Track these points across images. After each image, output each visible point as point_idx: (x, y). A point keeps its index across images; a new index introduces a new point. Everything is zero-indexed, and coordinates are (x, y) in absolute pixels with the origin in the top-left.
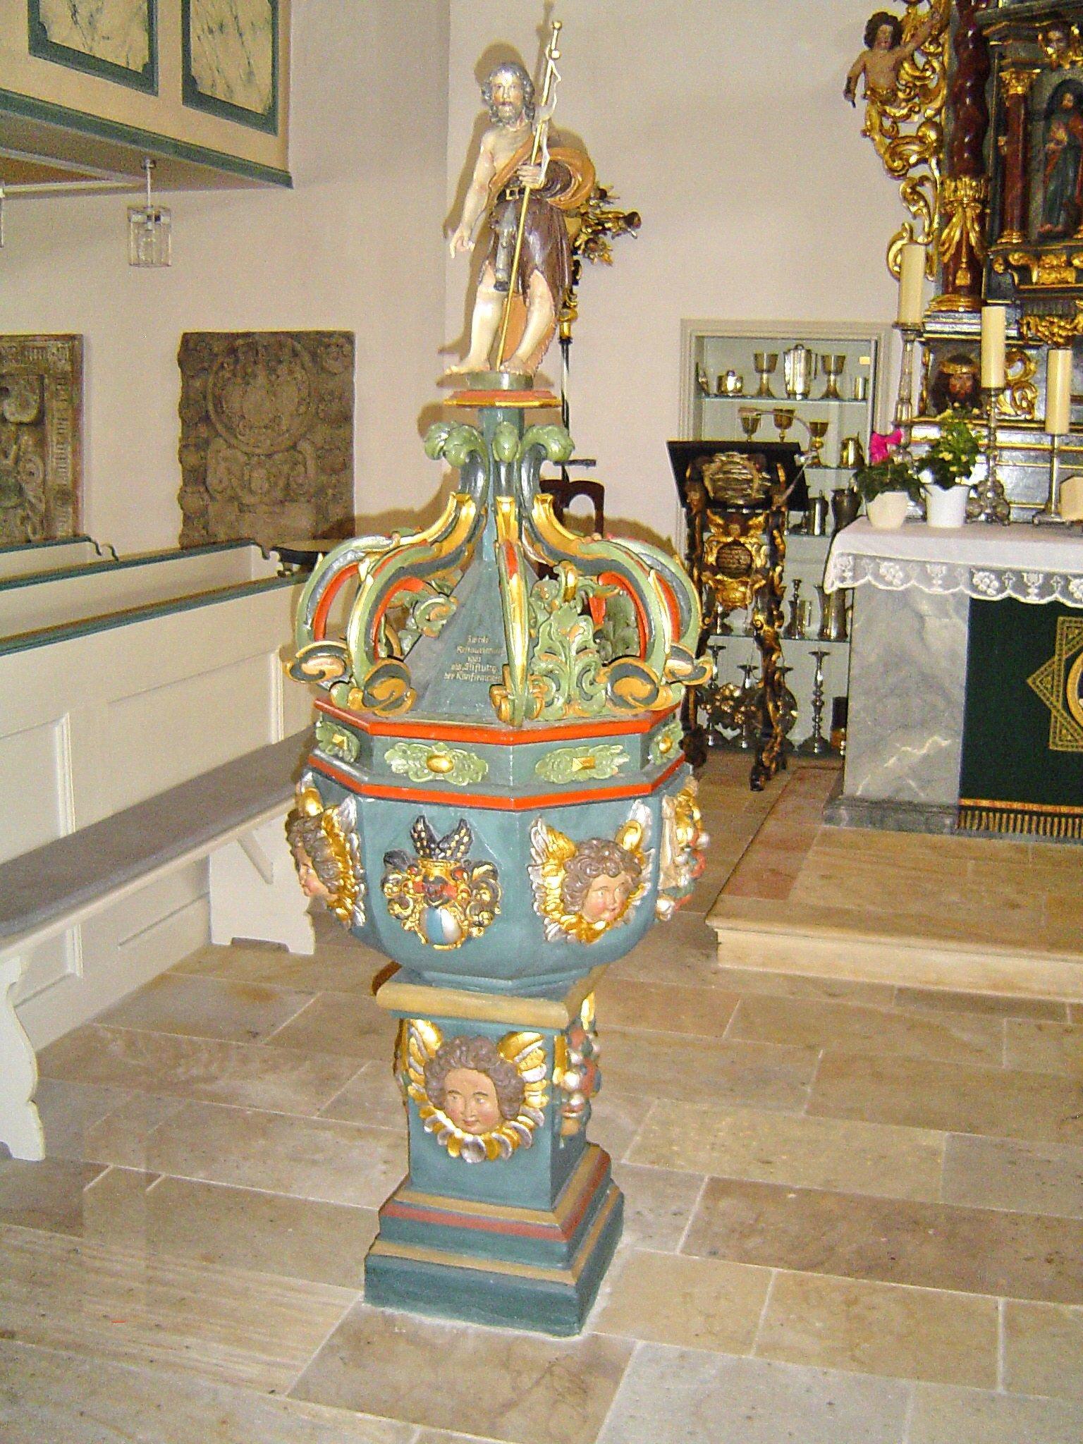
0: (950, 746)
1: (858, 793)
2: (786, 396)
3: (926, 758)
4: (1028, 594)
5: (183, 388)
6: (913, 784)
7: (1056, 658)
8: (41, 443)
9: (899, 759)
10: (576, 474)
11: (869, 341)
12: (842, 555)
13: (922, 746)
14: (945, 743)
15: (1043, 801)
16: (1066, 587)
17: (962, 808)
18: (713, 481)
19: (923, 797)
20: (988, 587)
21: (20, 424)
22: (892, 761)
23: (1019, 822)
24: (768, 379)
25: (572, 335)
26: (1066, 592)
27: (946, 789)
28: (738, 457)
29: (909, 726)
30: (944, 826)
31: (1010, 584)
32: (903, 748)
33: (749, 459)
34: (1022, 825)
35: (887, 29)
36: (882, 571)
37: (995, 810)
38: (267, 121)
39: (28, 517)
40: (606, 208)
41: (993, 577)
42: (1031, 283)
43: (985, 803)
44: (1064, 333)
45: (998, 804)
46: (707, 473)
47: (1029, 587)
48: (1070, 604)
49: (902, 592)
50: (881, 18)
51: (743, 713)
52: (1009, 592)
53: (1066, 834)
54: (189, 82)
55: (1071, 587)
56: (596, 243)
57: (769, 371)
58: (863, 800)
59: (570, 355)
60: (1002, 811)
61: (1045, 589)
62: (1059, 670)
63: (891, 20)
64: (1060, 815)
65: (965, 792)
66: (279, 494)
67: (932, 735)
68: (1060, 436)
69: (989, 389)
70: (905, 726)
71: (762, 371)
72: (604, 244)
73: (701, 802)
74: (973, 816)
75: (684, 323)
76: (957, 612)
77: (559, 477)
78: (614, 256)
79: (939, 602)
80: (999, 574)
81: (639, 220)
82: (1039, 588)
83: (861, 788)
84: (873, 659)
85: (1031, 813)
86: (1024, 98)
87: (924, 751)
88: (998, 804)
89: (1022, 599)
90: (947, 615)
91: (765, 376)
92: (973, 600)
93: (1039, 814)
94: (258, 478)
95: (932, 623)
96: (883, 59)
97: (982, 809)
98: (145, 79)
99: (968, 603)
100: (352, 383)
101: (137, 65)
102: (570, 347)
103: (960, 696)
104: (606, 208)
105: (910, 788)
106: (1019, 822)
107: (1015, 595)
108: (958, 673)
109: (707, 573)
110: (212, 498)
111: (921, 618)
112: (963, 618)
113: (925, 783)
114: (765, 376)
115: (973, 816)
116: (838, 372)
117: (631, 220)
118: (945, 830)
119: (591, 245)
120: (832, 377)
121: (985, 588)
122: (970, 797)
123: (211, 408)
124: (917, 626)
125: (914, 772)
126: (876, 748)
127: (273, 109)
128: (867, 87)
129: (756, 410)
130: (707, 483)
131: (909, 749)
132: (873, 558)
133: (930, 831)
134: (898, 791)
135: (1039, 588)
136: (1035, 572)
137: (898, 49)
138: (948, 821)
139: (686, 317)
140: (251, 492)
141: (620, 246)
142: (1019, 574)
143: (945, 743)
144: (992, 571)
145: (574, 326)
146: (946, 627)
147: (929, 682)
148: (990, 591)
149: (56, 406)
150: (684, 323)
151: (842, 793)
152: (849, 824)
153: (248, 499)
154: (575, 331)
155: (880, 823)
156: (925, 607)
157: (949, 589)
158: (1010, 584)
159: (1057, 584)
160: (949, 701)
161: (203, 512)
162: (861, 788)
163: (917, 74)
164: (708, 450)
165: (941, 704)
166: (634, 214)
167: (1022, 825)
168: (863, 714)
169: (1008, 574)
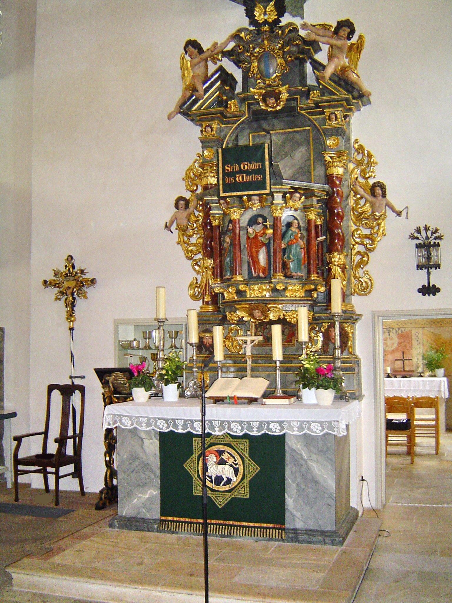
1: (124, 515)
2: (155, 348)
3: (148, 499)
4: (253, 431)
7: (194, 455)
10: (77, 382)
12: (109, 414)
13: (146, 494)
14: (155, 493)
15: (219, 519)
16: (268, 427)
19: (148, 516)
20: (237, 429)
23: (235, 530)
24: (149, 341)
25: (75, 326)
26: (268, 429)
27: (155, 513)
28: (120, 374)
29: (143, 485)
30: (155, 528)
31: (245, 427)
32: (139, 495)
33: (123, 375)
34: (185, 528)
35: (182, 202)
36: (123, 421)
37: (174, 521)
40: (84, 277)
41: (164, 422)
42: (246, 297)
43: (170, 518)
44: (236, 319)
45: (175, 519)
47: (179, 426)
48: (194, 432)
49: (123, 429)
50: (181, 198)
52: (171, 428)
53: (213, 532)
55: (194, 425)
56: (81, 290)
57: (149, 339)
58: (125, 517)
59: (74, 336)
60: (177, 522)
61: (260, 428)
62: (250, 461)
63: (184, 199)
64: (243, 526)
65: (162, 514)
67: (149, 489)
68: (220, 361)
69: (302, 342)
71: (146, 339)
72: (84, 290)
74: (165, 524)
76: (155, 437)
77: (71, 384)
78: (88, 295)
79: (148, 433)
80: (166, 420)
81: (96, 281)
82: (146, 423)
83: (124, 513)
85: (188, 523)
86: (219, 226)
87: (147, 496)
88: (175, 519)
89: (176, 431)
90: (152, 439)
91: (173, 340)
92: (160, 432)
93: (191, 523)
96: (183, 214)
97: (169, 521)
99: (158, 433)
100: (4, 348)
102: (73, 331)
103: (158, 472)
104: (84, 277)
106: (235, 530)
107: (173, 430)
108: (155, 463)
111: (142, 440)
112: (157, 439)
113: (148, 510)
114: (147, 340)
115: (165, 524)
116: (176, 337)
117: (93, 281)
119: (79, 291)
120: (147, 340)
121: (162, 427)
122: (164, 516)
124: (140, 442)
125: (144, 505)
126: (130, 494)
128: (178, 225)
129: (131, 354)
130: (111, 385)
132: (119, 415)
133: (149, 531)
135: (146, 423)
136: (180, 419)
137: (188, 210)
138: (156, 526)
141: (90, 291)
142: (248, 423)
143: (155, 493)
144: (164, 419)
145: (75, 323)
146: (151, 443)
147: (146, 466)
148: (317, 431)
151: (117, 514)
154: (76, 325)
155: (130, 528)
156: (143, 435)
158: (245, 427)
159: (189, 424)
160: (155, 475)
162: (124, 513)
163: (196, 219)
164: (109, 371)
165: (152, 476)
166: (94, 279)
167: (185, 528)
168: (123, 481)
169: (170, 421)
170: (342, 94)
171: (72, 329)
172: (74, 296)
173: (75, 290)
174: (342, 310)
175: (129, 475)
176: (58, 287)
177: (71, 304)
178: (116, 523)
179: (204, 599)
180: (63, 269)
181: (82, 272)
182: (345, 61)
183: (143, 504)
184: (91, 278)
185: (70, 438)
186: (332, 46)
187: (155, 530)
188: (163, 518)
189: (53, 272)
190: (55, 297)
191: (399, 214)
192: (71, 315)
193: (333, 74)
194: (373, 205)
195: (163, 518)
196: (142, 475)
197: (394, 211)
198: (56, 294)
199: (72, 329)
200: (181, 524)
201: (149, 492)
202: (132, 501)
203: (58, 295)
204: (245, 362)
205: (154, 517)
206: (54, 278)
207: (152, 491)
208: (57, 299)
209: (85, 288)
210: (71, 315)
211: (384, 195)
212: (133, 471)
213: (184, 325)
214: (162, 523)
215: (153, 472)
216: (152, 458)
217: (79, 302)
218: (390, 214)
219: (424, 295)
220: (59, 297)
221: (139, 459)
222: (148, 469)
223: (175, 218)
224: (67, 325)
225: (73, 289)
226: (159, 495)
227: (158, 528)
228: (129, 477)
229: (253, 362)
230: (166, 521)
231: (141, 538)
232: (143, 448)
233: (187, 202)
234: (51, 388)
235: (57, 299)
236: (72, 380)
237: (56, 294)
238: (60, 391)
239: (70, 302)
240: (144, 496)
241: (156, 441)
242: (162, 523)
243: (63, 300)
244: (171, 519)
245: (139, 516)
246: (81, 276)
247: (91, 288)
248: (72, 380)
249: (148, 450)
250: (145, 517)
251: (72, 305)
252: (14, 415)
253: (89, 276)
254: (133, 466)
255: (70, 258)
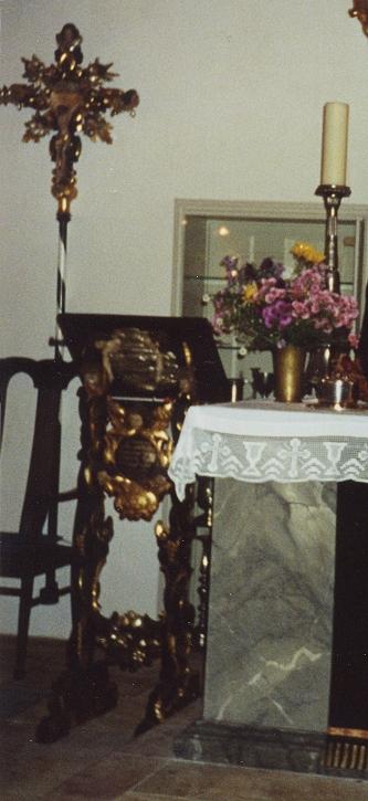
0: (318, 661)
1: (220, 717)
3: (293, 675)
5: (162, 569)
6: (280, 707)
9: (264, 677)
11: (354, 222)
14: (315, 658)
17: (330, 739)
18: (112, 361)
19: (291, 724)
22: (257, 677)
27: (314, 716)
29: (284, 635)
30: (309, 761)
32: (269, 663)
46: (105, 353)
51: (142, 649)
58: (222, 726)
65: (334, 720)
70: (271, 636)
74: (342, 750)
75: (178, 202)
76: (325, 498)
78: (113, 134)
84: (234, 554)
87: (291, 666)
90: (315, 504)
95: (299, 513)
103: (328, 597)
104: (106, 85)
105: (276, 710)
109: (104, 474)
111: (286, 505)
112: (329, 505)
113: (293, 706)
115: (342, 750)
118: (311, 767)
119: (91, 121)
124: (281, 513)
126: (240, 660)
130: (107, 365)
131: (275, 664)
133: (293, 768)
134: (263, 715)
138: (313, 756)
139: (181, 196)
145: (74, 203)
146: (313, 517)
147: (295, 580)
150: (178, 202)
151: (201, 718)
152: (204, 756)
154: (76, 207)
157: (257, 454)
160: (314, 599)
168: (224, 621)
171: (63, 218)
172: (76, 134)
173: (79, 118)
174: (298, 398)
175: (242, 605)
176: (34, 105)
177: (67, 152)
178: (196, 743)
180: (48, 60)
183: (277, 688)
184: (125, 89)
185: (67, 497)
187: (311, 767)
188: (337, 732)
189: (23, 65)
190: (24, 130)
192: (64, 183)
195: (337, 732)
196: (280, 605)
198: (27, 125)
199: (63, 218)
200: (347, 745)
201: (297, 655)
202: (249, 677)
203: (33, 126)
205: (307, 727)
206: (26, 82)
207: (307, 653)
208: (29, 136)
209: (106, 115)
210: (64, 183)
212: (255, 593)
213: (358, 224)
214: (331, 745)
215: (314, 599)
216: (312, 561)
217: (91, 148)
220: (36, 132)
221: (276, 559)
222: (298, 587)
224: (52, 205)
225: (75, 115)
226: (328, 664)
227: (319, 759)
228: (241, 611)
230: (343, 739)
231: (275, 792)
232: (287, 530)
235: (29, 136)
236: (57, 350)
237: (27, 125)
238: (32, 376)
239: (64, 149)
240: (282, 666)
241: (328, 510)
242: (331, 745)
243: (46, 141)
244: (359, 736)
245: (265, 723)
246: (96, 83)
247: (124, 116)
248: (57, 350)
249: (301, 536)
250: (284, 727)
251: (65, 156)
253: (122, 84)
254: (257, 577)
255: (69, 32)
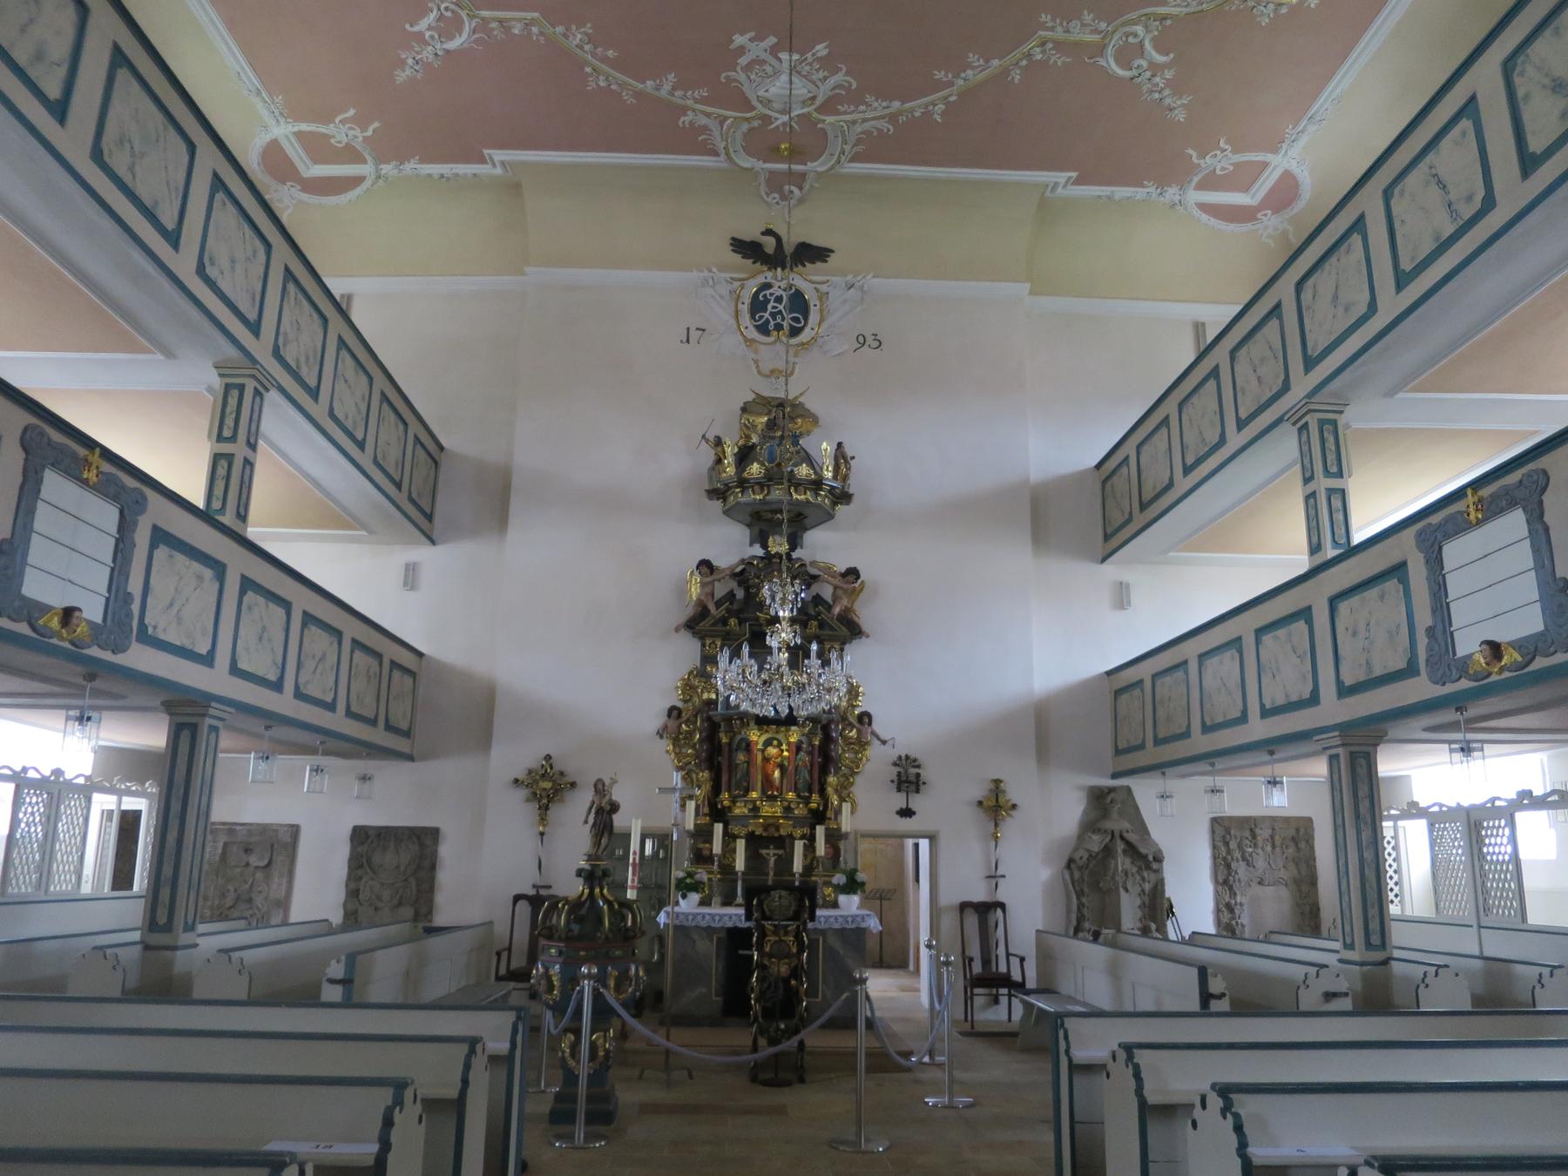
8: (268, 877)
21: (257, 867)
38: (407, 734)
39: (255, 914)
54: (234, 662)
66: (395, 901)
73: (595, 1070)
75: (938, 832)
94: (386, 895)
98: (277, 686)
101: (272, 677)
110: (361, 904)
123: (365, 861)
127: (410, 728)
140: (381, 901)
141: (521, 776)
149: (279, 859)
150: (938, 832)
153: (380, 905)
161: (356, 912)
170: (844, 630)
171: (542, 834)
179: (1563, 1017)
181: (562, 774)
182: (845, 602)
184: (571, 780)
186: (836, 588)
191: (884, 742)
193: (839, 614)
194: (859, 732)
197: (879, 739)
199: (542, 834)
204: (767, 874)
211: (870, 724)
218: (877, 742)
219: (901, 816)
223: (665, 727)
229: (775, 875)
233: (680, 711)
234: (517, 898)
252: (1003, 876)
